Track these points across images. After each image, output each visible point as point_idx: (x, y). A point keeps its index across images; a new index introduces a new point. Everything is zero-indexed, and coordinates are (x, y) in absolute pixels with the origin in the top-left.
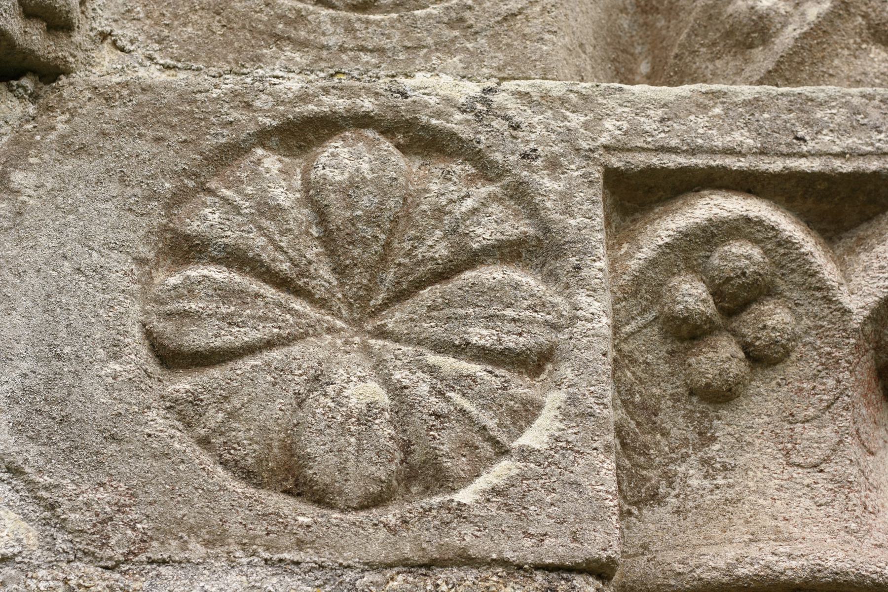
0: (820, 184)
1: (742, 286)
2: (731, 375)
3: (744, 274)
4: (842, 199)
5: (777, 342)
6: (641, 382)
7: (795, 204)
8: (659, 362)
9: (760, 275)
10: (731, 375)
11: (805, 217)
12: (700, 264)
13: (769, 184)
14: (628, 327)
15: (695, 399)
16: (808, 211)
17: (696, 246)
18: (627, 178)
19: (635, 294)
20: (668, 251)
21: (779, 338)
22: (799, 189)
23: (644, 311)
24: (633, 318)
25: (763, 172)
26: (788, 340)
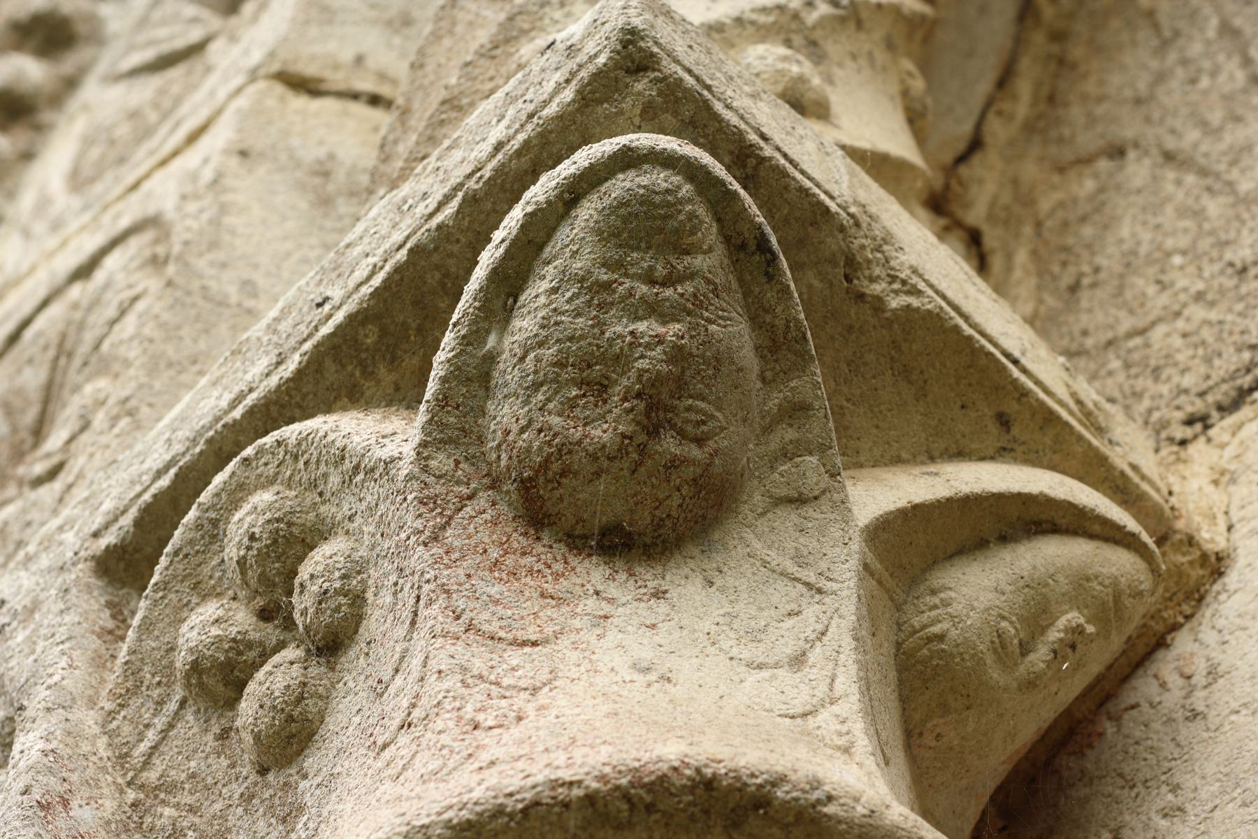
0: (366, 336)
1: (262, 556)
2: (277, 694)
3: (252, 537)
4: (420, 330)
5: (325, 592)
6: (192, 810)
7: (368, 393)
8: (210, 761)
9: (278, 520)
10: (277, 694)
11: (400, 401)
12: (220, 579)
13: (304, 396)
14: (142, 745)
15: (271, 777)
16: (397, 389)
17: (200, 558)
18: (136, 550)
19: (134, 691)
20: (161, 594)
21: (326, 585)
22: (350, 368)
23: (160, 703)
24: (147, 726)
25: (279, 386)
26: (344, 577)
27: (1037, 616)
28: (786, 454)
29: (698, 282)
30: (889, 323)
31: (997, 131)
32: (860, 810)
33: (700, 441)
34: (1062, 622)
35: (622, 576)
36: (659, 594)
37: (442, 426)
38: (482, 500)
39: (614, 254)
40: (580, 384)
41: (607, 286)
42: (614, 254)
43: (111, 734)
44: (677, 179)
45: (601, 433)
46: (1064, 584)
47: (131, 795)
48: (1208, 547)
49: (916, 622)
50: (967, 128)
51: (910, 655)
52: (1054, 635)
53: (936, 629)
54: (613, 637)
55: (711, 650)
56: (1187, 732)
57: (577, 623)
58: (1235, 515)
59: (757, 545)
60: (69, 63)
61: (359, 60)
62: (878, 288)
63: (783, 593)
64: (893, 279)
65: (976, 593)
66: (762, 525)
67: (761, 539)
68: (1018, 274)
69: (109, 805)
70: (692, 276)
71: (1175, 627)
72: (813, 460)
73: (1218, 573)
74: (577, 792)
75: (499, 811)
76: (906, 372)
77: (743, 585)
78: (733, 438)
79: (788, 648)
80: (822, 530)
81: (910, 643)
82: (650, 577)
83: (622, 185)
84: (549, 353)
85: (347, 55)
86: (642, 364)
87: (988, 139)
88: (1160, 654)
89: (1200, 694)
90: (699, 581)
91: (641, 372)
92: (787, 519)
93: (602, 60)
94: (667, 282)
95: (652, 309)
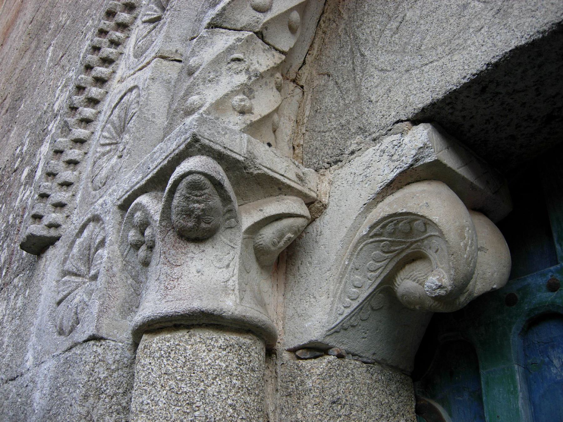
19: (123, 242)
27: (281, 237)
28: (228, 219)
29: (207, 195)
30: (254, 177)
31: (309, 59)
32: (230, 313)
33: (209, 223)
34: (286, 237)
35: (197, 247)
36: (203, 251)
37: (163, 217)
38: (171, 232)
39: (189, 191)
40: (186, 215)
41: (189, 197)
42: (189, 191)
43: (120, 250)
44: (200, 176)
45: (190, 224)
46: (287, 229)
47: (124, 263)
48: (324, 203)
49: (257, 241)
50: (302, 60)
51: (256, 247)
52: (285, 239)
53: (260, 243)
54: (194, 263)
55: (212, 265)
56: (315, 245)
57: (187, 260)
58: (331, 194)
59: (222, 238)
60: (135, 12)
61: (177, 51)
62: (251, 170)
63: (226, 249)
64: (255, 167)
65: (268, 234)
66: (224, 233)
67: (223, 237)
68: (308, 102)
69: (120, 265)
70: (205, 194)
71: (317, 218)
72: (233, 220)
73: (325, 208)
74: (179, 314)
75: (167, 316)
76: (259, 184)
77: (219, 247)
78: (216, 220)
79: (226, 263)
80: (235, 234)
81: (256, 245)
82: (202, 247)
83: (189, 178)
84: (180, 209)
85: (174, 50)
86: (196, 213)
87: (307, 62)
88: (314, 222)
89: (318, 237)
90: (211, 247)
91: (196, 215)
92: (229, 231)
93: (189, 140)
94: (200, 196)
95: (198, 202)
